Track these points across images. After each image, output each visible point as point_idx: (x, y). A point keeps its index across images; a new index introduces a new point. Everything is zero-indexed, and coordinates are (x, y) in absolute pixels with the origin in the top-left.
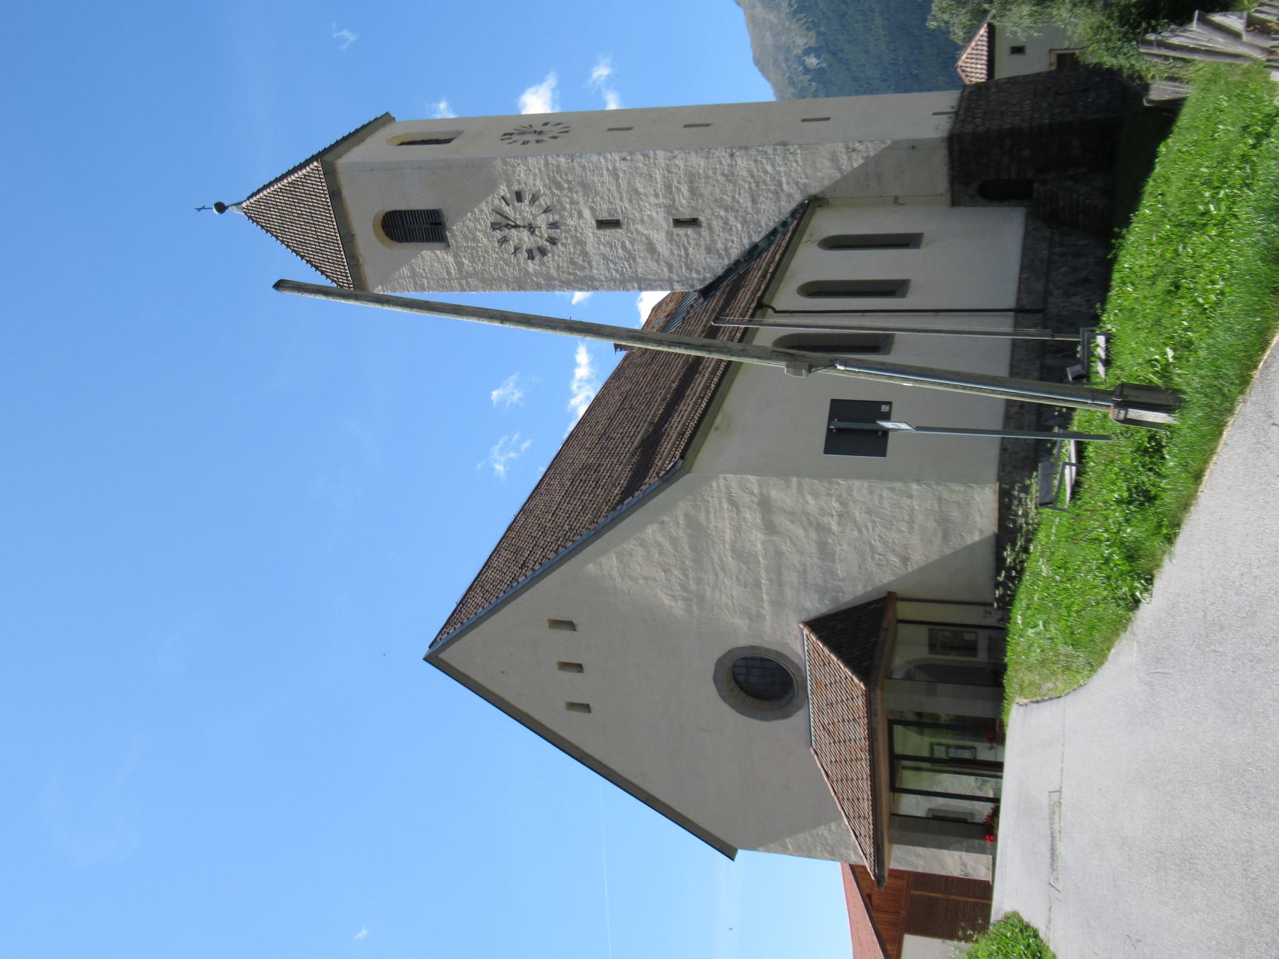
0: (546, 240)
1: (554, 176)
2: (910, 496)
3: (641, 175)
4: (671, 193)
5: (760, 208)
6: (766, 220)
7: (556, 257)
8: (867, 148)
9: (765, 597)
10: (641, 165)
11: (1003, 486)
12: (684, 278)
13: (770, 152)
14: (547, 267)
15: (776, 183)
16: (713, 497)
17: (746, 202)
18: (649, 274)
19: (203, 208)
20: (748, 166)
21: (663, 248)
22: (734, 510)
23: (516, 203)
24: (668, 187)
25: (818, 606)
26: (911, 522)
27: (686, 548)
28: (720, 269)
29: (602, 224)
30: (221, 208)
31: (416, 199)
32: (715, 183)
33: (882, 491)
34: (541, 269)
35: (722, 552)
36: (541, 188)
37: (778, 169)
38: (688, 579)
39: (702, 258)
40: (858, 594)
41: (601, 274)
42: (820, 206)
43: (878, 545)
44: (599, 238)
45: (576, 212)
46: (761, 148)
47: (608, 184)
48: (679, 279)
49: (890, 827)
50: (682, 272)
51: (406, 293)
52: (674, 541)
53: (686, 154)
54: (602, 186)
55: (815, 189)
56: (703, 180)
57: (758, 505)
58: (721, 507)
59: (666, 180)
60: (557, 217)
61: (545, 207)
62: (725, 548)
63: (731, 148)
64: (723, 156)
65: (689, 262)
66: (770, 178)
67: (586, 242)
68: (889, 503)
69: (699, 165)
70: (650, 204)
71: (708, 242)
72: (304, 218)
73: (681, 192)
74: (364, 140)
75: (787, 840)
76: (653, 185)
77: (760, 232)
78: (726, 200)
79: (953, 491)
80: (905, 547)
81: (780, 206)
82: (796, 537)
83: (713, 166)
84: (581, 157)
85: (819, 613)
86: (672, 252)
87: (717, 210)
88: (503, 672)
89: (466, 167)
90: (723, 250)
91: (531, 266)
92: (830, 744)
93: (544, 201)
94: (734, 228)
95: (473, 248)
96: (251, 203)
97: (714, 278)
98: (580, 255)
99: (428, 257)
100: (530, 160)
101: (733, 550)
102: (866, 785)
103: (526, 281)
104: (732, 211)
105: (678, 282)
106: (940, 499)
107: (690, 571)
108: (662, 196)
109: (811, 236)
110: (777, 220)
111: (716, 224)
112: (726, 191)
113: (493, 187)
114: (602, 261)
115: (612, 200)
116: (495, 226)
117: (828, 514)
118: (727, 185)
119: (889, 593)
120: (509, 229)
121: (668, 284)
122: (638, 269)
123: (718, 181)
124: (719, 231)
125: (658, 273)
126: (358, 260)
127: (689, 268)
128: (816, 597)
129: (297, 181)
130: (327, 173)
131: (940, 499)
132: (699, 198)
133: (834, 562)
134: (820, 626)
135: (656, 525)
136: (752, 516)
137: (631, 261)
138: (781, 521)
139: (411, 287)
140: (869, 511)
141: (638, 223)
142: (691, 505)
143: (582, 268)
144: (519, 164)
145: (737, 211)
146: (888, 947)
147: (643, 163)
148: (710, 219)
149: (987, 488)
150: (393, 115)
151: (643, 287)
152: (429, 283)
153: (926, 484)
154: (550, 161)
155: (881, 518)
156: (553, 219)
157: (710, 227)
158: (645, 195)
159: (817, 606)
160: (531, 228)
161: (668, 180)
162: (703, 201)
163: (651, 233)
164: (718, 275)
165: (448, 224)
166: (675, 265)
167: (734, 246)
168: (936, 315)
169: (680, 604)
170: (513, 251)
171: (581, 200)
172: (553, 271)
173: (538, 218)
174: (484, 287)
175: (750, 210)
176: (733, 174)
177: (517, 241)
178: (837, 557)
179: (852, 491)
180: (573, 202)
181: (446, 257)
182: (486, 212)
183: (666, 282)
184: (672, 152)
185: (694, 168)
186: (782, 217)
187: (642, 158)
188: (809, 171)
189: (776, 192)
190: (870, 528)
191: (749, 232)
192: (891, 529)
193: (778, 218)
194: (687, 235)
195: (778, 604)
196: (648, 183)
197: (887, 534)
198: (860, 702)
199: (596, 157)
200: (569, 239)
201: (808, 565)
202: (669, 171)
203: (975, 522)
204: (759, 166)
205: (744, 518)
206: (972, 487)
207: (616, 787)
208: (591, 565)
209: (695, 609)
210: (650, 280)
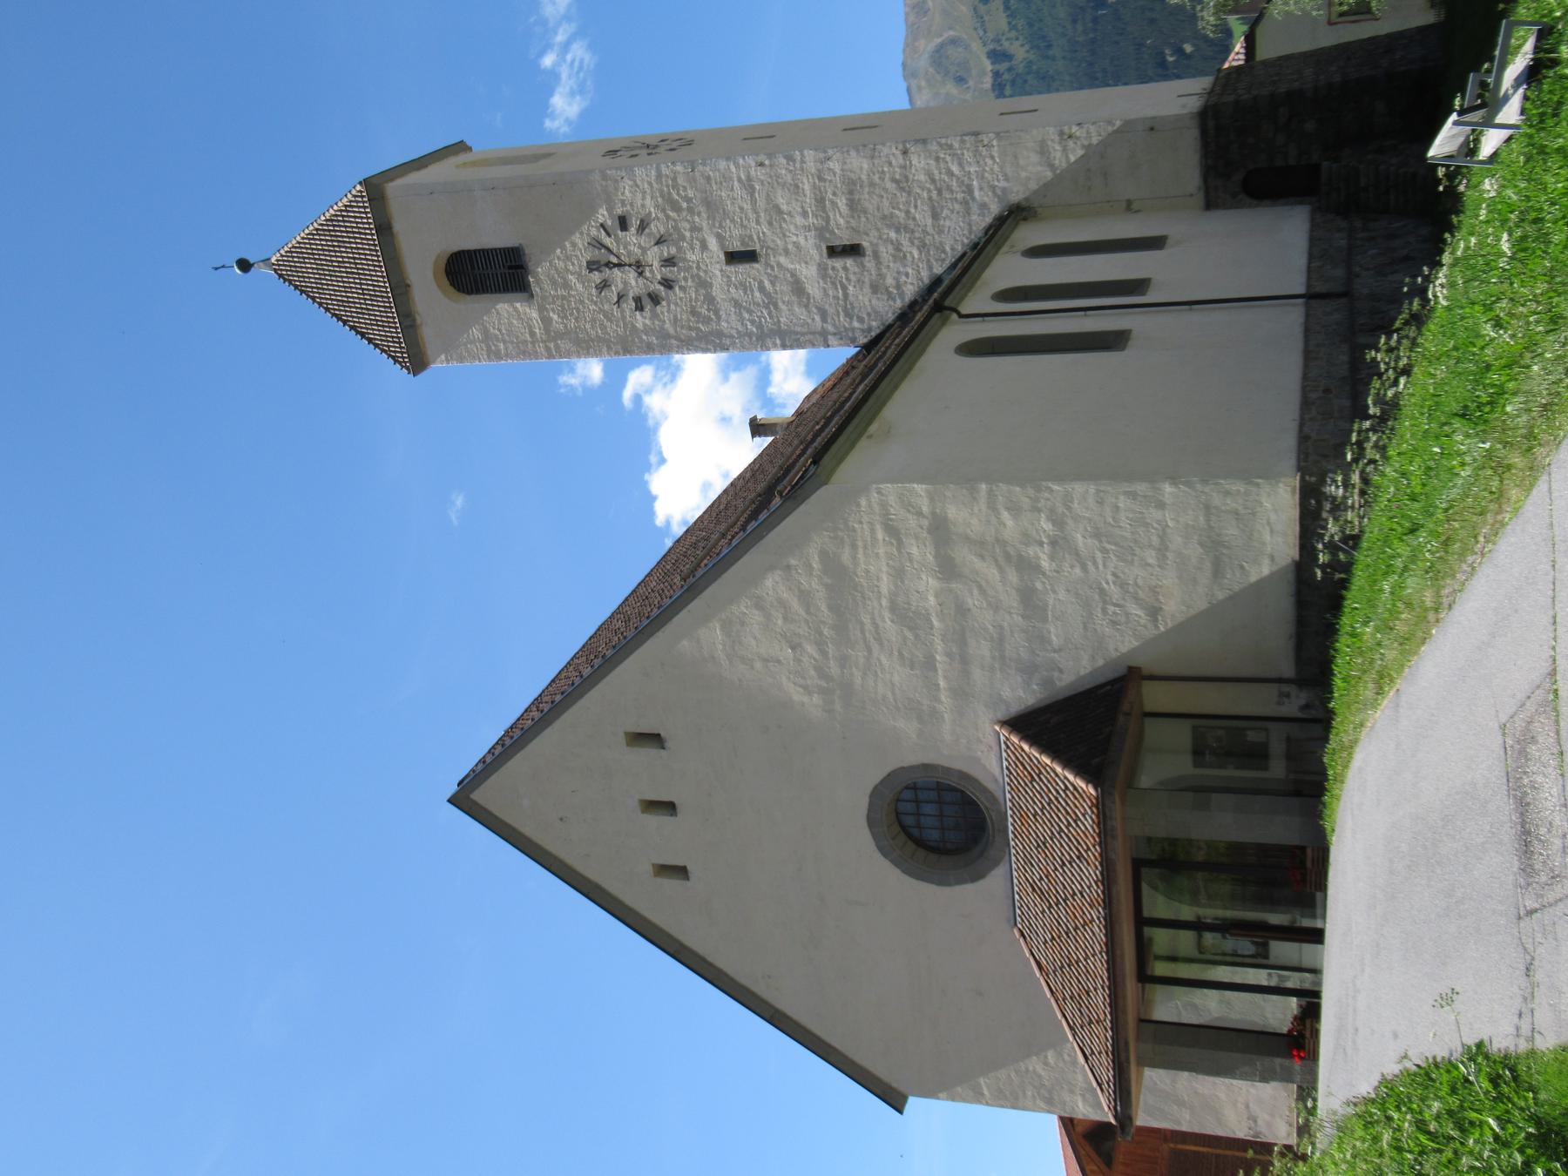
0: (659, 283)
1: (669, 193)
2: (1161, 505)
3: (783, 185)
4: (824, 209)
5: (943, 226)
6: (952, 242)
7: (672, 307)
8: (1088, 133)
9: (942, 683)
10: (784, 172)
11: (1307, 478)
12: (842, 329)
13: (956, 145)
14: (660, 320)
15: (964, 188)
16: (861, 523)
17: (924, 217)
18: (795, 325)
19: (223, 267)
20: (926, 167)
21: (814, 289)
22: (895, 542)
23: (619, 232)
24: (820, 201)
25: (1022, 694)
26: (1162, 550)
27: (824, 607)
28: (890, 315)
29: (733, 257)
30: (245, 265)
31: (490, 234)
32: (883, 193)
33: (1117, 498)
34: (653, 323)
35: (876, 612)
36: (652, 210)
37: (967, 169)
38: (828, 659)
39: (866, 299)
40: (1082, 672)
41: (732, 328)
42: (1025, 219)
43: (1114, 591)
44: (728, 277)
45: (698, 243)
46: (943, 141)
47: (740, 201)
48: (835, 331)
49: (1138, 1039)
50: (839, 321)
51: (477, 362)
52: (805, 597)
53: (843, 153)
54: (733, 203)
55: (1016, 196)
56: (867, 190)
57: (929, 532)
58: (874, 539)
59: (818, 193)
60: (673, 251)
61: (658, 236)
62: (881, 605)
63: (904, 142)
64: (893, 154)
65: (849, 306)
66: (957, 182)
67: (711, 283)
68: (1127, 518)
69: (861, 168)
70: (796, 226)
71: (874, 277)
72: (346, 267)
73: (838, 208)
74: (427, 166)
75: (982, 1080)
76: (800, 199)
77: (944, 260)
78: (897, 217)
79: (1227, 493)
80: (1154, 590)
81: (970, 220)
82: (987, 582)
83: (880, 169)
84: (704, 164)
85: (1023, 707)
86: (826, 294)
87: (886, 231)
88: (561, 819)
89: (554, 184)
90: (894, 287)
91: (640, 320)
92: (1043, 912)
93: (656, 228)
94: (908, 255)
95: (564, 298)
96: (282, 256)
97: (882, 327)
98: (704, 303)
99: (506, 311)
100: (637, 171)
101: (893, 608)
102: (1099, 966)
103: (633, 340)
104: (906, 232)
105: (835, 334)
106: (1207, 508)
107: (830, 645)
108: (813, 215)
109: (1013, 246)
110: (966, 241)
111: (885, 250)
112: (898, 203)
113: (589, 211)
114: (733, 309)
115: (745, 222)
116: (593, 266)
117: (1036, 541)
118: (899, 194)
120: (611, 269)
121: (820, 339)
122: (781, 319)
123: (886, 190)
124: (889, 262)
125: (808, 323)
126: (414, 320)
127: (848, 315)
128: (1019, 679)
129: (337, 216)
130: (374, 199)
131: (1207, 508)
132: (862, 215)
133: (1045, 620)
134: (1027, 724)
135: (779, 572)
136: (920, 551)
137: (772, 309)
138: (963, 555)
139: (482, 355)
140: (1097, 535)
141: (780, 254)
142: (830, 537)
143: (707, 320)
144: (622, 178)
145: (913, 232)
147: (786, 169)
148: (877, 245)
149: (1281, 485)
150: (469, 143)
151: (788, 344)
152: (506, 349)
153: (1185, 484)
154: (664, 173)
155: (1116, 544)
156: (669, 253)
157: (876, 255)
158: (790, 214)
159: (1022, 695)
160: (639, 267)
161: (820, 191)
162: (867, 219)
163: (798, 267)
164: (887, 323)
165: (531, 266)
166: (831, 311)
167: (910, 281)
168: (1191, 310)
169: (816, 699)
170: (616, 300)
171: (704, 224)
172: (668, 326)
173: (649, 252)
174: (579, 352)
175: (929, 229)
176: (906, 178)
177: (621, 286)
178: (1050, 613)
179: (1072, 502)
180: (695, 229)
181: (528, 310)
182: (581, 246)
183: (817, 336)
184: (825, 152)
185: (855, 173)
186: (973, 237)
187: (784, 161)
188: (1009, 170)
189: (965, 203)
190: (1100, 562)
191: (928, 261)
192: (1132, 562)
193: (967, 238)
194: (845, 269)
195: (962, 693)
196: (793, 197)
197: (1126, 571)
198: (1089, 823)
199: (725, 163)
200: (690, 280)
201: (1006, 624)
202: (821, 179)
203: (1264, 544)
204: (942, 165)
205: (909, 554)
206: (1258, 485)
207: (727, 997)
208: (685, 643)
209: (838, 707)
210: (797, 333)
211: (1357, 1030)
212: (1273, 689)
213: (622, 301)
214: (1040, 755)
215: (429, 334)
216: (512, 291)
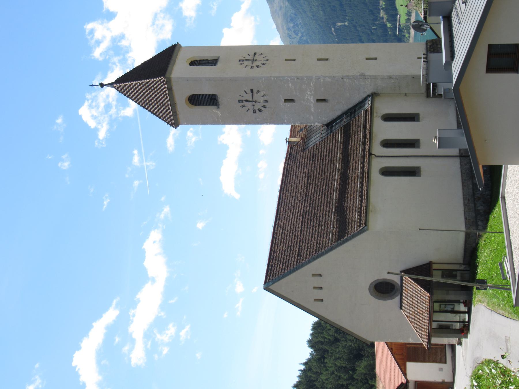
70: (308, 94)
116: (240, 101)
119: (430, 262)
126: (177, 113)
146: (402, 368)
181: (217, 111)
212: (459, 265)
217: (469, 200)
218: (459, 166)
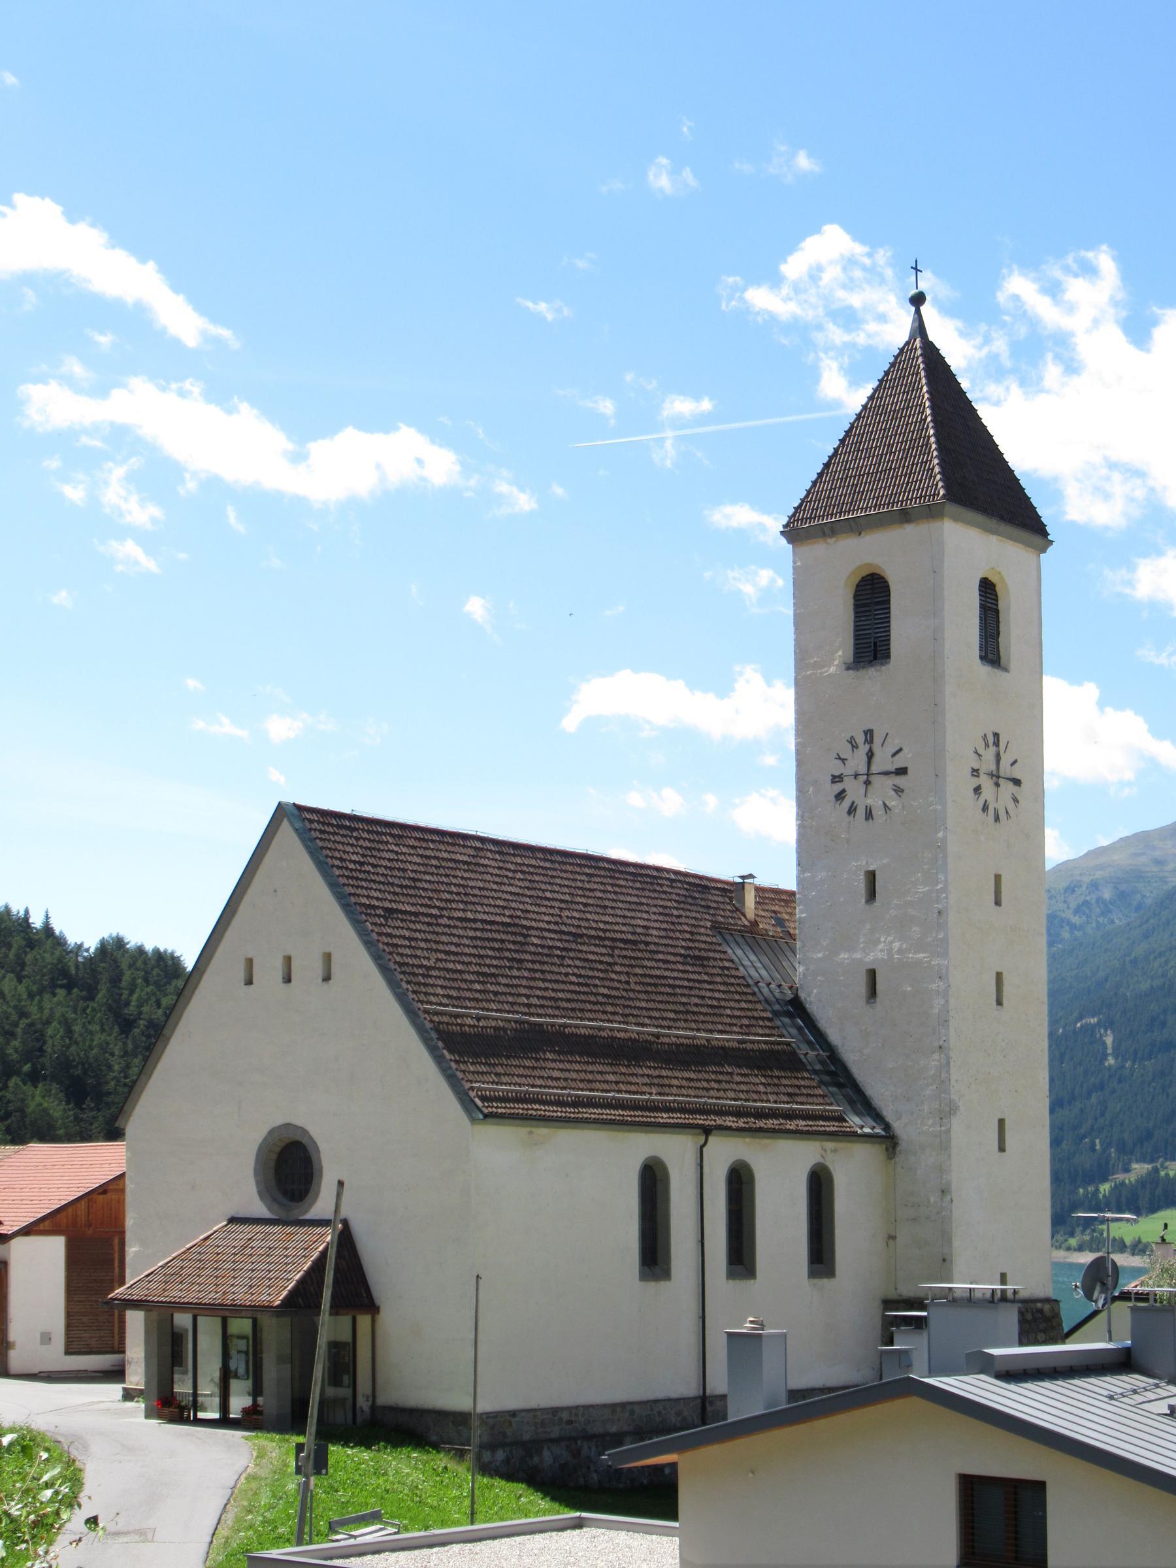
70: (891, 942)
88: (275, 891)
181: (836, 663)
211: (120, 1462)
212: (369, 1392)
213: (840, 761)
214: (320, 1252)
215: (819, 549)
216: (856, 645)
217: (570, 1422)
218: (674, 1395)
